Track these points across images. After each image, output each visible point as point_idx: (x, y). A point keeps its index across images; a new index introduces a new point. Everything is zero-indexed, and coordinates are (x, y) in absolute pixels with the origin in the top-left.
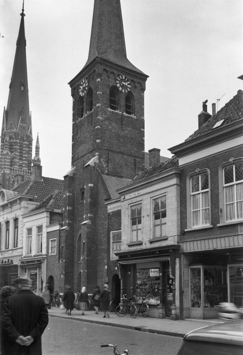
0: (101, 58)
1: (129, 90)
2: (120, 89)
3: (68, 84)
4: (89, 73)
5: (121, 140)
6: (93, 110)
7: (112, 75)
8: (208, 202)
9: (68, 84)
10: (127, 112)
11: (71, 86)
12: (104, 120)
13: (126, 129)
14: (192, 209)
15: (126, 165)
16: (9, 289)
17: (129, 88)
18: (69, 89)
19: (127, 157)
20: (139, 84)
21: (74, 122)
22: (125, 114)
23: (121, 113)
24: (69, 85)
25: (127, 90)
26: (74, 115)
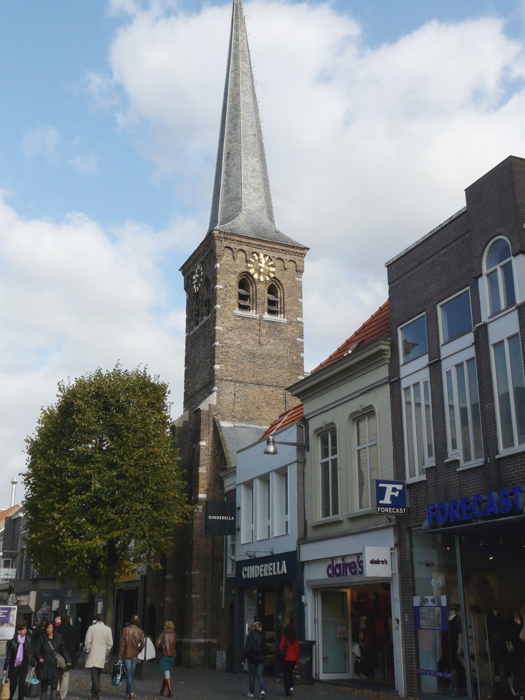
1: (272, 275)
2: (256, 276)
3: (179, 270)
4: (205, 254)
7: (241, 255)
9: (179, 270)
10: (271, 312)
15: (268, 404)
16: (261, 426)
17: (272, 272)
18: (180, 279)
19: (269, 390)
20: (292, 263)
23: (258, 315)
24: (180, 272)
25: (269, 276)
26: (188, 321)
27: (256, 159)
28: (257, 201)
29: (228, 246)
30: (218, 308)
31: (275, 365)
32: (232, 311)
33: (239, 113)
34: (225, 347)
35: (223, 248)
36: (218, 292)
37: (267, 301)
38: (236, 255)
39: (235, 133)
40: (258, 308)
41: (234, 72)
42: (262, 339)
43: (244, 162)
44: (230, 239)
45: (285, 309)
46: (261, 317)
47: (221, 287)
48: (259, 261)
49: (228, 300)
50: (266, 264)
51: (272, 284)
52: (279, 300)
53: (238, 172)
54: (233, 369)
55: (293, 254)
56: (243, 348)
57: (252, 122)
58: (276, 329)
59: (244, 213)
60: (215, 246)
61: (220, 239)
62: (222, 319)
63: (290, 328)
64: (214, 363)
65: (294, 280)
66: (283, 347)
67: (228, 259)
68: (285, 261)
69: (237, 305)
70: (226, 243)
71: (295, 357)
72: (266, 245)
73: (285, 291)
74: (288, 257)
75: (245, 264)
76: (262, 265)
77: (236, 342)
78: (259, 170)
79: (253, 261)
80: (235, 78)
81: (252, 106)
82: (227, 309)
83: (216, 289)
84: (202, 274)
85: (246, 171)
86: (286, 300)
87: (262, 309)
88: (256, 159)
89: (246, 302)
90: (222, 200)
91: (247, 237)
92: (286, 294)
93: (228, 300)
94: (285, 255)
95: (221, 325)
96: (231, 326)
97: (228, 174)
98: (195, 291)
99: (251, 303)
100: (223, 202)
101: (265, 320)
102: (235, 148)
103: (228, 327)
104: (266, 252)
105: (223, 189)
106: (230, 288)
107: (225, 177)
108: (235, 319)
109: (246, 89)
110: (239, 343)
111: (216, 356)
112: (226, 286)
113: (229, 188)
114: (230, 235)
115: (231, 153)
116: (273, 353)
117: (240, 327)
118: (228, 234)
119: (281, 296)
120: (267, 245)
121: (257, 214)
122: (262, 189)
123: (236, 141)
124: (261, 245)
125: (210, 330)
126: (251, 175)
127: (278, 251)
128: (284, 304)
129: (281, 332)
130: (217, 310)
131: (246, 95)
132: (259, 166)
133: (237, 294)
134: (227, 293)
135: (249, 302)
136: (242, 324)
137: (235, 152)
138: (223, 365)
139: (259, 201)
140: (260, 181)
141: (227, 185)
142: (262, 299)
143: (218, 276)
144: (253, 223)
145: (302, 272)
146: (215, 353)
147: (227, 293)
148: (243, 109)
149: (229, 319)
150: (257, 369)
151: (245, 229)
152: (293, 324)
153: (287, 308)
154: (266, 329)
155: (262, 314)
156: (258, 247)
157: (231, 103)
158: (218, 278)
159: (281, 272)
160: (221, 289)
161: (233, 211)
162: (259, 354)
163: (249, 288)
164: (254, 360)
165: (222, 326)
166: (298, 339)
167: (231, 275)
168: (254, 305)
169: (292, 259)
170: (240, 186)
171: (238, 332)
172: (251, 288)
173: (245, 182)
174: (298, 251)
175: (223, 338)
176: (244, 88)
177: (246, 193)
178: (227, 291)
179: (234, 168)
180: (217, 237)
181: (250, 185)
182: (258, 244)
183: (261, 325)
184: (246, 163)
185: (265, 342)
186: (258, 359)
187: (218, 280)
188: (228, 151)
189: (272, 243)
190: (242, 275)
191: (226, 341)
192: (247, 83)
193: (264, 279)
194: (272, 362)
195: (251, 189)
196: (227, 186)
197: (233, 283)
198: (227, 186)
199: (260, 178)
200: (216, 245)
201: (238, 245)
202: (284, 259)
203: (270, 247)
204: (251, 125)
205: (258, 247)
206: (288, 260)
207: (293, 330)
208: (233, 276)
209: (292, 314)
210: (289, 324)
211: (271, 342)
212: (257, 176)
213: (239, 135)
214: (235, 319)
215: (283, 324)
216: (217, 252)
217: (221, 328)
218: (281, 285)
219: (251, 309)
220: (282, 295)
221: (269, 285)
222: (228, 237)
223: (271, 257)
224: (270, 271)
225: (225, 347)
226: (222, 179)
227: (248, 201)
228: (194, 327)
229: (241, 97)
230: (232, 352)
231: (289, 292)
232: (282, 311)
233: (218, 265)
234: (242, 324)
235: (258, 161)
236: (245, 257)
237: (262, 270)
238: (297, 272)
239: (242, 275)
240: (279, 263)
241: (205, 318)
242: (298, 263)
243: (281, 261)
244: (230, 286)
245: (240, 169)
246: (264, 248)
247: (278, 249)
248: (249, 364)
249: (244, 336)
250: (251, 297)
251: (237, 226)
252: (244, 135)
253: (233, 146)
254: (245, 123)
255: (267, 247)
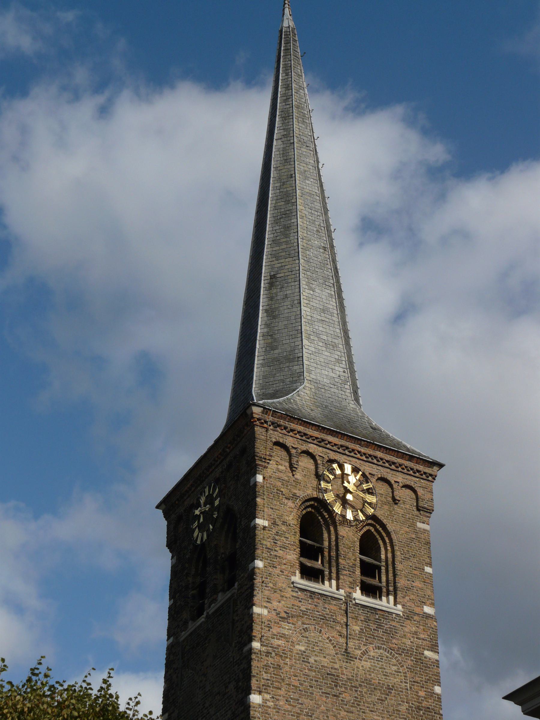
0: (264, 408)
2: (337, 509)
3: (157, 507)
5: (346, 697)
6: (236, 584)
7: (305, 463)
8: (304, 585)
9: (157, 507)
11: (167, 515)
12: (277, 619)
13: (364, 653)
14: (357, 699)
20: (408, 492)
21: (171, 640)
22: (358, 595)
24: (160, 512)
27: (329, 291)
28: (333, 367)
29: (281, 441)
30: (259, 568)
31: (379, 706)
32: (288, 577)
33: (294, 207)
34: (273, 654)
35: (270, 444)
36: (259, 534)
37: (358, 564)
38: (297, 462)
39: (286, 242)
40: (341, 577)
41: (283, 140)
42: (351, 644)
43: (305, 293)
44: (285, 428)
45: (399, 585)
46: (349, 596)
47: (266, 523)
48: (344, 476)
49: (280, 553)
50: (358, 486)
51: (369, 531)
52: (383, 564)
53: (295, 310)
54: (289, 708)
55: (411, 472)
56: (312, 660)
57: (319, 225)
58: (380, 626)
59: (307, 385)
60: (252, 438)
61: (265, 425)
62: (267, 593)
63: (410, 627)
64: (248, 691)
65: (413, 525)
66: (395, 668)
67: (280, 467)
68: (395, 486)
69: (297, 565)
70: (276, 435)
71: (422, 694)
72: (357, 447)
73: (396, 548)
74: (399, 478)
75: (315, 482)
76: (351, 487)
77: (297, 647)
78: (335, 312)
79: (332, 477)
80: (284, 149)
81: (318, 198)
82: (277, 571)
83: (255, 527)
84: (217, 503)
85: (309, 310)
86: (399, 566)
87: (351, 580)
88: (329, 291)
89: (316, 563)
90: (261, 362)
91: (319, 426)
92: (398, 553)
93: (280, 553)
94: (394, 473)
95: (265, 604)
96: (285, 609)
97: (271, 313)
98: (199, 542)
99: (327, 565)
100: (263, 365)
101: (357, 604)
102: (286, 267)
103: (279, 610)
104: (358, 463)
105: (262, 342)
106: (284, 528)
107: (266, 319)
108: (295, 594)
109: (307, 169)
110: (303, 649)
111: (254, 672)
112: (274, 523)
113: (275, 339)
114: (285, 420)
115: (278, 276)
116: (376, 678)
117: (304, 613)
118: (282, 417)
119: (387, 557)
120: (360, 449)
121: (332, 390)
122: (341, 346)
123: (289, 256)
124: (347, 448)
125: (236, 618)
126: (319, 317)
127: (381, 463)
128: (395, 575)
129: (391, 633)
130: (257, 571)
131: (306, 178)
132: (335, 305)
133: (298, 543)
134: (277, 537)
135: (322, 562)
136: (310, 607)
137: (286, 274)
138: (268, 696)
139: (336, 368)
140: (338, 331)
141: (270, 335)
142: (350, 559)
143: (258, 500)
144: (326, 407)
145: (429, 511)
146: (250, 666)
147: (277, 537)
148: (301, 201)
149: (283, 594)
150: (343, 713)
151: (313, 414)
152: (416, 618)
153: (401, 582)
154: (359, 623)
155: (350, 590)
156: (341, 450)
157: (278, 191)
158: (258, 503)
159: (386, 507)
160: (264, 528)
161: (283, 381)
162: (345, 677)
163: (322, 534)
164: (335, 691)
165: (266, 607)
166: (427, 653)
167: (286, 501)
168: (334, 570)
169: (408, 483)
170: (299, 335)
171: (300, 623)
172: (326, 535)
173: (308, 328)
174: (421, 468)
175: (269, 634)
176: (302, 168)
177: (310, 348)
178: (277, 534)
179: (285, 304)
180: (259, 419)
181: (318, 335)
182: (340, 443)
183: (349, 615)
184: (310, 296)
185: (359, 652)
186: (343, 689)
187: (260, 507)
188: (272, 273)
189: (369, 444)
190: (308, 504)
191: (276, 642)
192: (308, 160)
193: (354, 517)
194: (374, 698)
195: (321, 344)
196: (271, 336)
197: (291, 518)
198: (271, 336)
199: (336, 326)
200: (257, 436)
201: (300, 442)
202: (392, 479)
203: (365, 454)
204: (317, 231)
205: (341, 450)
206: (401, 485)
207: (416, 633)
208: (290, 504)
209: (412, 597)
210: (408, 618)
211: (372, 654)
212: (331, 321)
213: (296, 244)
214: (295, 594)
215: (394, 615)
216: (257, 450)
217: (265, 612)
218: (388, 534)
219: (326, 578)
220: (390, 555)
221: (362, 532)
222: (282, 422)
223: (367, 474)
224: (366, 502)
225: (273, 654)
226: (260, 323)
227: (315, 365)
228: (190, 622)
229: (297, 182)
230: (287, 668)
231: (406, 550)
232: (391, 588)
233: (259, 478)
234: (310, 607)
235: (332, 295)
236: (313, 467)
237: (349, 497)
238: (418, 510)
239: (308, 504)
240: (382, 488)
241: (221, 598)
242: (420, 492)
243: (386, 486)
244: (284, 523)
245: (298, 305)
246: (352, 454)
247: (382, 459)
248: (324, 699)
249: (313, 635)
250: (326, 554)
251: (295, 406)
252: (305, 245)
253: (283, 264)
254: (305, 225)
255: (359, 452)
